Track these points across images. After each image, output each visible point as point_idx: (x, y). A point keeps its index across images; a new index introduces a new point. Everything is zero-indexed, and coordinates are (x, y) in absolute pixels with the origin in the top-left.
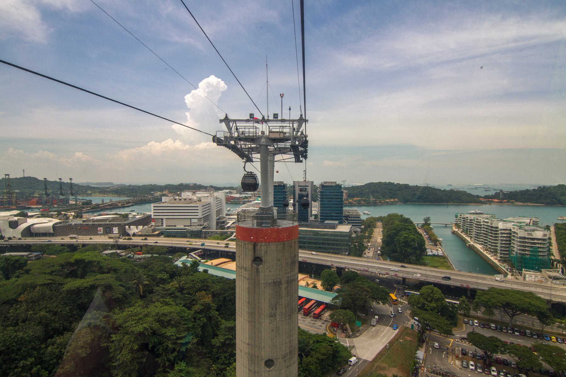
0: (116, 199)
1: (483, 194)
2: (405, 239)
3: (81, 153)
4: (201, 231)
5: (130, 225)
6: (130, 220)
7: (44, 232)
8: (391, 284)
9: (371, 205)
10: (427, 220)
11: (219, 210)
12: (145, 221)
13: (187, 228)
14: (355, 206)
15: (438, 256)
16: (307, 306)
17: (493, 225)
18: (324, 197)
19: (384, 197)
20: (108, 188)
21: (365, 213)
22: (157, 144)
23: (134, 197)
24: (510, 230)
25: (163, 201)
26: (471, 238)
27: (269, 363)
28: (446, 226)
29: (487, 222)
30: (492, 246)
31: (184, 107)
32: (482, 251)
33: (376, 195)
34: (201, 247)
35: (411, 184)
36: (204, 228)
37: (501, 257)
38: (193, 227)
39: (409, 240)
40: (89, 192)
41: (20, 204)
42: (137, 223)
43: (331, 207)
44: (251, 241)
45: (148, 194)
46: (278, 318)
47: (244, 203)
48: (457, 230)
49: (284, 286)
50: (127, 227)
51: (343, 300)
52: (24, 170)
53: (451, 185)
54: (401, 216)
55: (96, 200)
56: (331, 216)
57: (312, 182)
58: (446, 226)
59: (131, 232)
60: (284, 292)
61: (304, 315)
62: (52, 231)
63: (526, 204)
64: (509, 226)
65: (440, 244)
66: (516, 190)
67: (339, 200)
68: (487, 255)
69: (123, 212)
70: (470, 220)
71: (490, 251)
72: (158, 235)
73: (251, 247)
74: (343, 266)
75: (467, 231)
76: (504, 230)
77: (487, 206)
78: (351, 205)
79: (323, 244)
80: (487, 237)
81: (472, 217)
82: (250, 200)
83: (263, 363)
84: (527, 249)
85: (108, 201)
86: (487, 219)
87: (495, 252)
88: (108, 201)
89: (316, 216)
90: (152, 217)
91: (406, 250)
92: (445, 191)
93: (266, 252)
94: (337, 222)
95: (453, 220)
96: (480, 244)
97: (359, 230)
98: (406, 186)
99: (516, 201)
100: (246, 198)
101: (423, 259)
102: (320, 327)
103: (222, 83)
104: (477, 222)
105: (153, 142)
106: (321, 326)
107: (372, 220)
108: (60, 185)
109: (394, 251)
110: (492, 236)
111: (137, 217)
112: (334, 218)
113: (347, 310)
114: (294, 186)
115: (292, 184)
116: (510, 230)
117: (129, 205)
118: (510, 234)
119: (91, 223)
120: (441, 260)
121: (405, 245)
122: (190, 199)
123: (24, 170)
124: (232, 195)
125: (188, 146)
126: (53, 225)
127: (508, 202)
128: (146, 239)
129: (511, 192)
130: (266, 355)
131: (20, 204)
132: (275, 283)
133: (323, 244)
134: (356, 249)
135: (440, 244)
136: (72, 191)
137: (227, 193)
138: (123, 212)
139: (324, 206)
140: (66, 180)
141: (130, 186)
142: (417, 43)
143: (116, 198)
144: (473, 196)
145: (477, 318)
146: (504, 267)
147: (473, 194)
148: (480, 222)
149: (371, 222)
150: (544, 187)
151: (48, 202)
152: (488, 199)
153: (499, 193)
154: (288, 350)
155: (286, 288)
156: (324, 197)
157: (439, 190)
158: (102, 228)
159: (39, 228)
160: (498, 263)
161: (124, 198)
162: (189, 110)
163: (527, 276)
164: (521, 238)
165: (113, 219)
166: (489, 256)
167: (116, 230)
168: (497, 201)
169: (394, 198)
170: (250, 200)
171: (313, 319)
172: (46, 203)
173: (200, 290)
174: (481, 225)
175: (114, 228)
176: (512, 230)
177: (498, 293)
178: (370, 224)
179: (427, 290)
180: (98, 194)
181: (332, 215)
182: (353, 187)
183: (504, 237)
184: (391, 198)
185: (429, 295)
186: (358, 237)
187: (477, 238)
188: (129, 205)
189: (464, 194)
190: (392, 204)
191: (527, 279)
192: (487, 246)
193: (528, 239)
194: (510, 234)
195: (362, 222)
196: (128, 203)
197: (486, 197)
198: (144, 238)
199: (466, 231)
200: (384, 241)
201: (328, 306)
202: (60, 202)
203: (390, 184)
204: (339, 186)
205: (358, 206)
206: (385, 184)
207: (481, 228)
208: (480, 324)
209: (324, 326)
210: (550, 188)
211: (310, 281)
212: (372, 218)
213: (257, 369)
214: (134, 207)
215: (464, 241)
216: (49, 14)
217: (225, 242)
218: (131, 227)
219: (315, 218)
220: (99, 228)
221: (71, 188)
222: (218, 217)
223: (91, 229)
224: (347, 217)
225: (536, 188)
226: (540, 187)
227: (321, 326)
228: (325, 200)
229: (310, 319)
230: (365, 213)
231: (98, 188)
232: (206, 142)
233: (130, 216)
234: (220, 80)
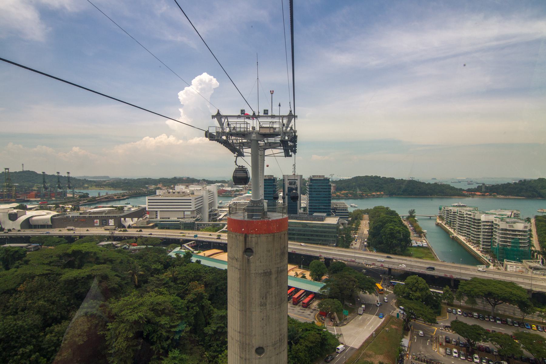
0: (112, 192)
1: (466, 188)
2: (390, 230)
3: (78, 148)
4: (194, 223)
5: (125, 217)
6: (126, 213)
7: (42, 224)
8: (377, 274)
9: (358, 198)
10: (412, 212)
11: (211, 203)
12: (140, 213)
13: (180, 220)
14: (342, 199)
15: (422, 247)
16: (296, 296)
17: (476, 218)
18: (313, 190)
19: (370, 190)
20: (105, 181)
21: (352, 205)
22: (152, 139)
23: (129, 190)
24: (492, 222)
25: (157, 194)
26: (454, 229)
27: (260, 351)
28: (430, 218)
29: (470, 215)
30: (475, 237)
31: (177, 103)
32: (465, 242)
33: (363, 188)
34: (194, 239)
35: (397, 177)
36: (197, 220)
37: (483, 248)
38: (186, 220)
39: (395, 232)
40: (86, 185)
41: (19, 197)
42: (132, 215)
43: (319, 200)
44: (243, 233)
45: (143, 188)
46: (268, 307)
47: (235, 196)
48: (440, 222)
49: (274, 276)
50: (122, 219)
51: (331, 289)
52: (23, 165)
53: (435, 179)
54: (387, 208)
55: (93, 193)
56: (319, 209)
57: (301, 176)
58: (430, 218)
59: (126, 224)
60: (274, 282)
61: (294, 304)
62: (50, 223)
63: (508, 197)
64: (491, 218)
65: (425, 235)
66: (498, 183)
67: (327, 193)
68: (470, 246)
69: (119, 204)
70: (454, 212)
71: (473, 243)
72: (152, 227)
73: (242, 238)
74: (331, 257)
75: (450, 223)
76: (486, 222)
77: (470, 199)
78: (339, 198)
79: (312, 235)
80: (470, 229)
81: (456, 209)
82: (241, 193)
83: (254, 350)
84: (508, 240)
85: (104, 194)
86: (470, 211)
87: (477, 243)
88: (104, 194)
89: (305, 208)
90: (147, 209)
91: (392, 242)
92: (429, 184)
93: (257, 243)
94: (325, 214)
95: (437, 212)
96: (463, 236)
97: (346, 222)
98: (392, 180)
99: (498, 194)
100: (237, 191)
101: (408, 250)
102: (309, 316)
103: (214, 81)
104: (460, 214)
105: (148, 137)
106: (310, 315)
107: (359, 212)
108: (58, 179)
109: (380, 243)
110: (474, 228)
111: (133, 209)
112: (322, 210)
113: (335, 300)
114: (284, 180)
115: (282, 178)
116: (492, 222)
117: (125, 198)
118: (492, 226)
119: (88, 215)
120: (426, 251)
121: (390, 236)
122: (183, 192)
123: (23, 165)
124: (224, 188)
125: (181, 141)
126: (51, 217)
127: (490, 195)
128: (141, 231)
129: (493, 186)
130: (256, 342)
131: (19, 197)
132: (265, 273)
133: (312, 235)
134: (344, 241)
135: (425, 235)
136: (69, 185)
137: (219, 186)
138: (119, 204)
139: (313, 199)
140: (63, 174)
141: (125, 179)
142: (403, 41)
143: (112, 191)
144: (457, 189)
145: (460, 307)
146: (486, 258)
147: (456, 187)
148: (463, 215)
149: (358, 214)
150: (525, 180)
151: (47, 195)
152: (471, 193)
153: (481, 186)
154: (278, 338)
155: (276, 278)
156: (313, 190)
157: (423, 183)
158: (98, 220)
159: (37, 220)
160: (480, 254)
161: (120, 192)
162: (182, 106)
163: (509, 266)
164: (502, 230)
165: (109, 212)
166: (472, 247)
167: (112, 222)
168: (480, 194)
169: (380, 191)
170: (241, 193)
171: (302, 308)
172: (44, 196)
173: (192, 280)
174: (464, 217)
175: (110, 220)
176: (494, 222)
177: (480, 283)
178: (357, 217)
179: (412, 280)
180: (94, 187)
181: (320, 207)
182: (340, 180)
183: (487, 229)
184: (377, 191)
185: (413, 285)
186: (345, 229)
187: (460, 230)
188: (125, 198)
189: (448, 187)
190: (378, 197)
191: (508, 270)
192: (469, 237)
193: (509, 230)
194: (492, 226)
195: (350, 214)
196: (123, 196)
197: (469, 190)
198: (139, 230)
199: (449, 223)
200: (370, 233)
201: (316, 296)
202: (58, 195)
203: (376, 177)
204: (327, 180)
205: (345, 199)
206: (371, 177)
207: (464, 220)
208: (463, 312)
209: (312, 314)
210: (530, 181)
211: (299, 271)
212: (359, 210)
213: (247, 356)
214: (130, 200)
215: (448, 233)
216: (47, 14)
217: (217, 233)
218: (127, 219)
219: (304, 211)
220: (95, 221)
221: (69, 181)
222: (210, 210)
223: (88, 221)
224: (335, 210)
225: (517, 182)
226: (521, 181)
227: (310, 315)
228: (313, 193)
229: (299, 308)
230: (352, 205)
231: (94, 182)
232: (199, 137)
233: (126, 209)
234: (212, 77)
